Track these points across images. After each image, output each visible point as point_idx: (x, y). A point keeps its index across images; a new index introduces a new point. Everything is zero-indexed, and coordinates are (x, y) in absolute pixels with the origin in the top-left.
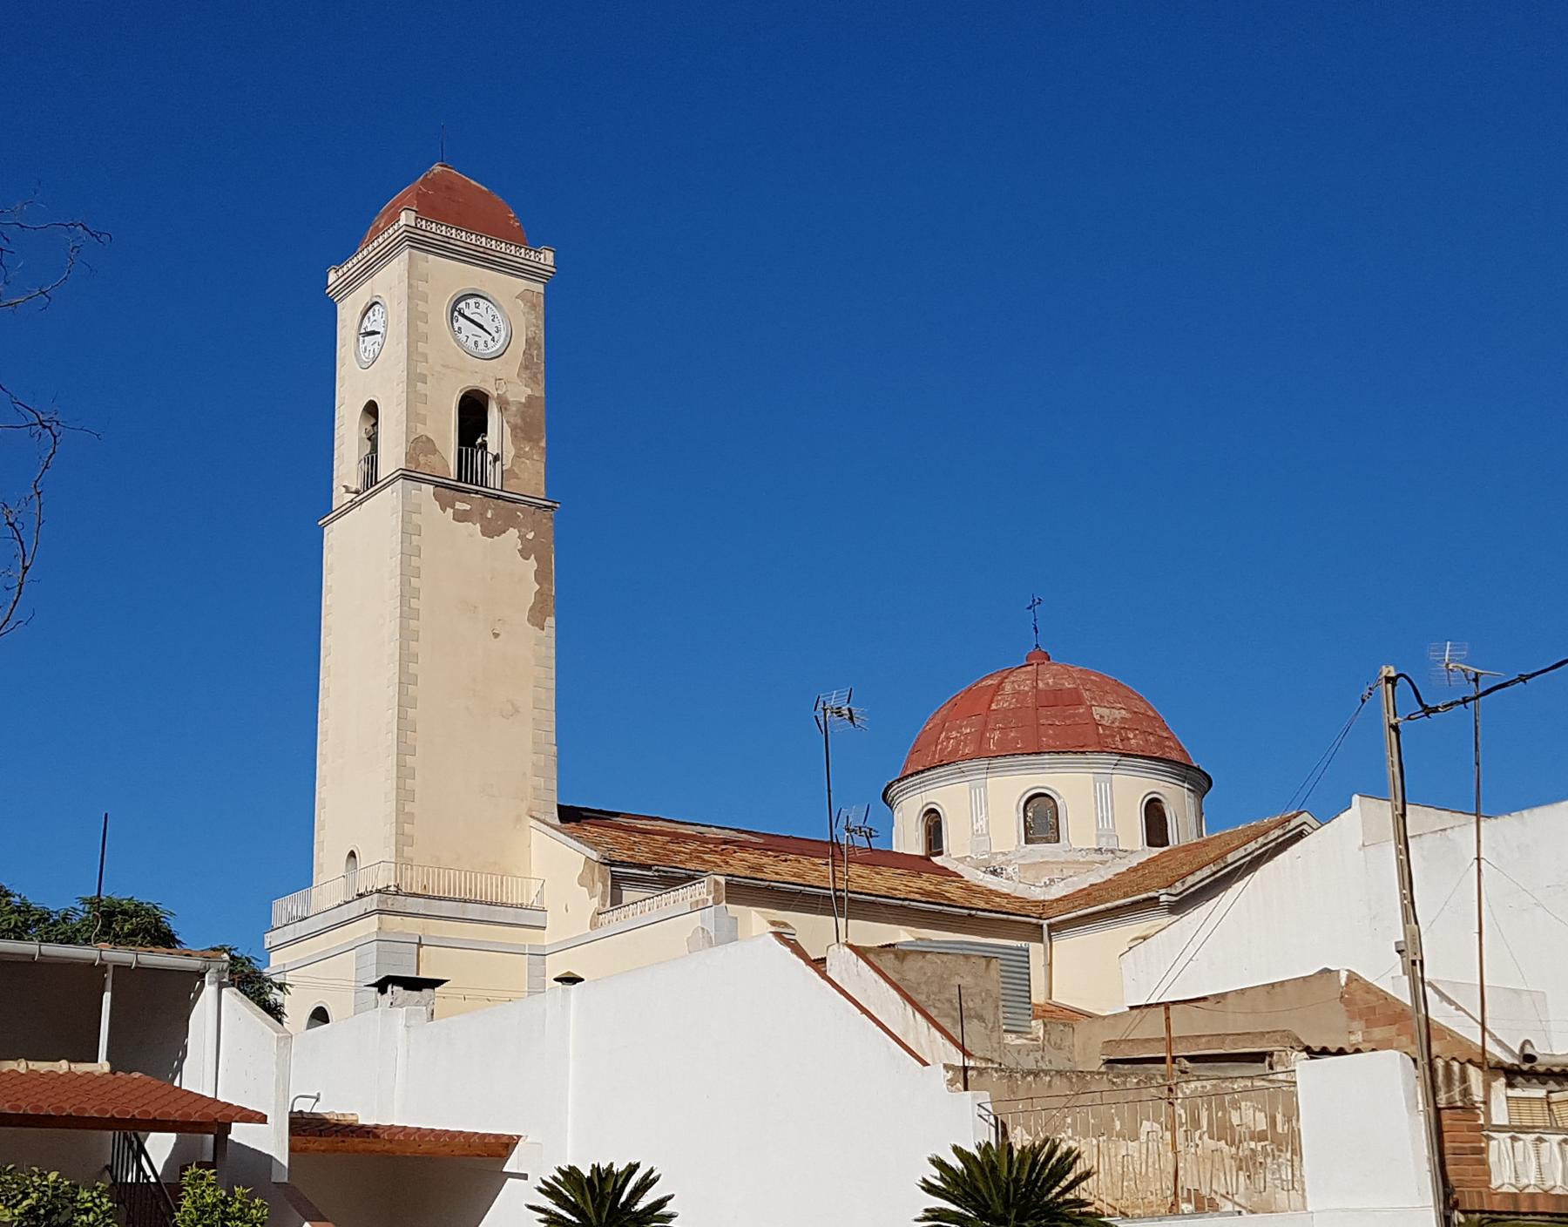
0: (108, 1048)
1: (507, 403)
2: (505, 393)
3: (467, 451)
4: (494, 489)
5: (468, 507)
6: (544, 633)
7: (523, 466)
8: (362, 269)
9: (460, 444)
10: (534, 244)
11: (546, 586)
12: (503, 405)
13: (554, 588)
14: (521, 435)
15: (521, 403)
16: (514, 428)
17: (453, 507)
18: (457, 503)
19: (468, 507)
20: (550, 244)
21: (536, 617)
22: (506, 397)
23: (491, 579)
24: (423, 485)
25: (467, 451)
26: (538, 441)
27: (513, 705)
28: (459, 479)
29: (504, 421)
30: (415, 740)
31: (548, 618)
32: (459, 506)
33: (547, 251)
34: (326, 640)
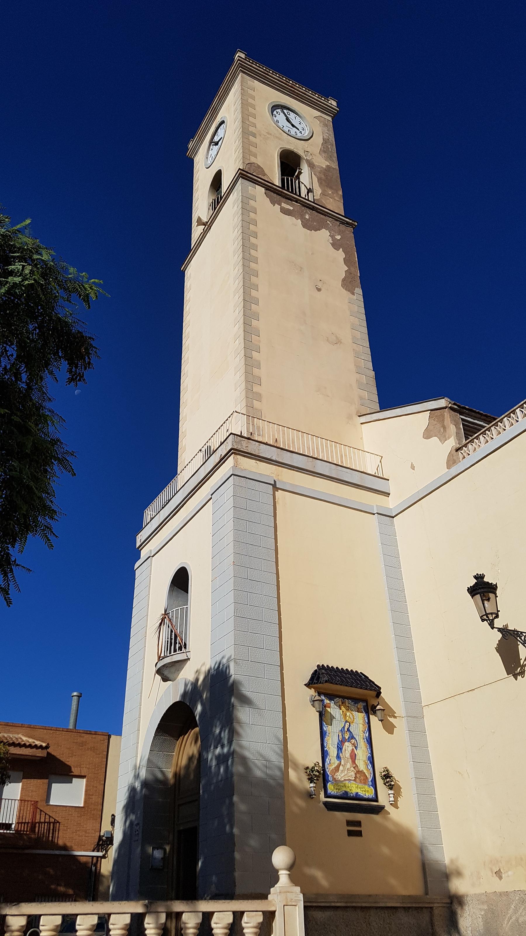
0: (356, 830)
1: (314, 165)
2: (311, 159)
3: (288, 180)
4: (308, 200)
5: (292, 208)
6: (355, 297)
7: (328, 201)
8: (214, 104)
9: (282, 175)
10: (326, 95)
11: (352, 269)
12: (311, 165)
13: (359, 271)
14: (323, 183)
15: (322, 167)
16: (319, 179)
17: (280, 204)
18: (282, 203)
19: (292, 208)
20: (334, 98)
21: (347, 284)
22: (312, 161)
23: (312, 254)
24: (255, 80)
25: (288, 180)
26: (337, 191)
27: (336, 337)
28: (283, 187)
29: (312, 173)
30: (260, 341)
31: (356, 289)
32: (283, 205)
33: (332, 100)
34: (188, 295)
